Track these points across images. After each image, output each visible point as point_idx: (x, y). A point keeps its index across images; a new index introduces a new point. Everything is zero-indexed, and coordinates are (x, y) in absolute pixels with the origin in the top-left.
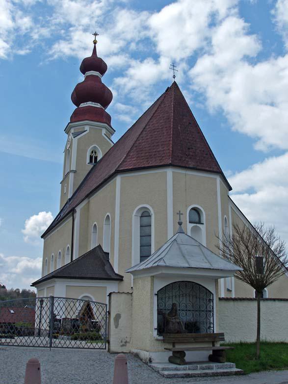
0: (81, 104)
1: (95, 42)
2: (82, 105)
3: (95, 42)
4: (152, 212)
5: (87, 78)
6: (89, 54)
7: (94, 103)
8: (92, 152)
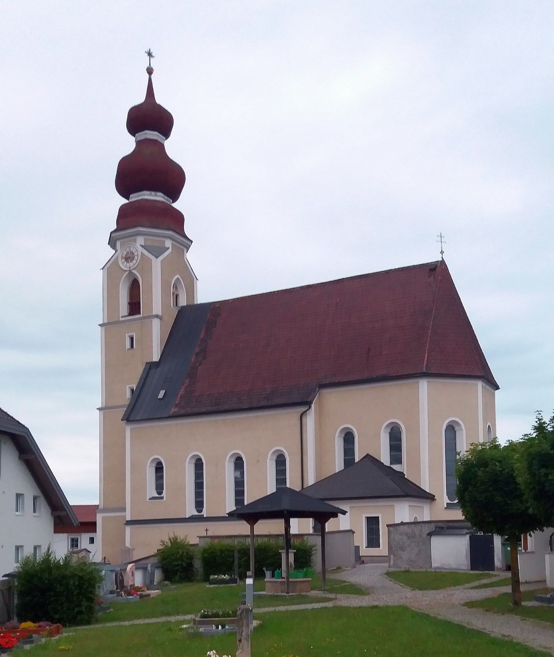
1: (150, 71)
2: (135, 197)
3: (150, 71)
5: (138, 143)
6: (140, 98)
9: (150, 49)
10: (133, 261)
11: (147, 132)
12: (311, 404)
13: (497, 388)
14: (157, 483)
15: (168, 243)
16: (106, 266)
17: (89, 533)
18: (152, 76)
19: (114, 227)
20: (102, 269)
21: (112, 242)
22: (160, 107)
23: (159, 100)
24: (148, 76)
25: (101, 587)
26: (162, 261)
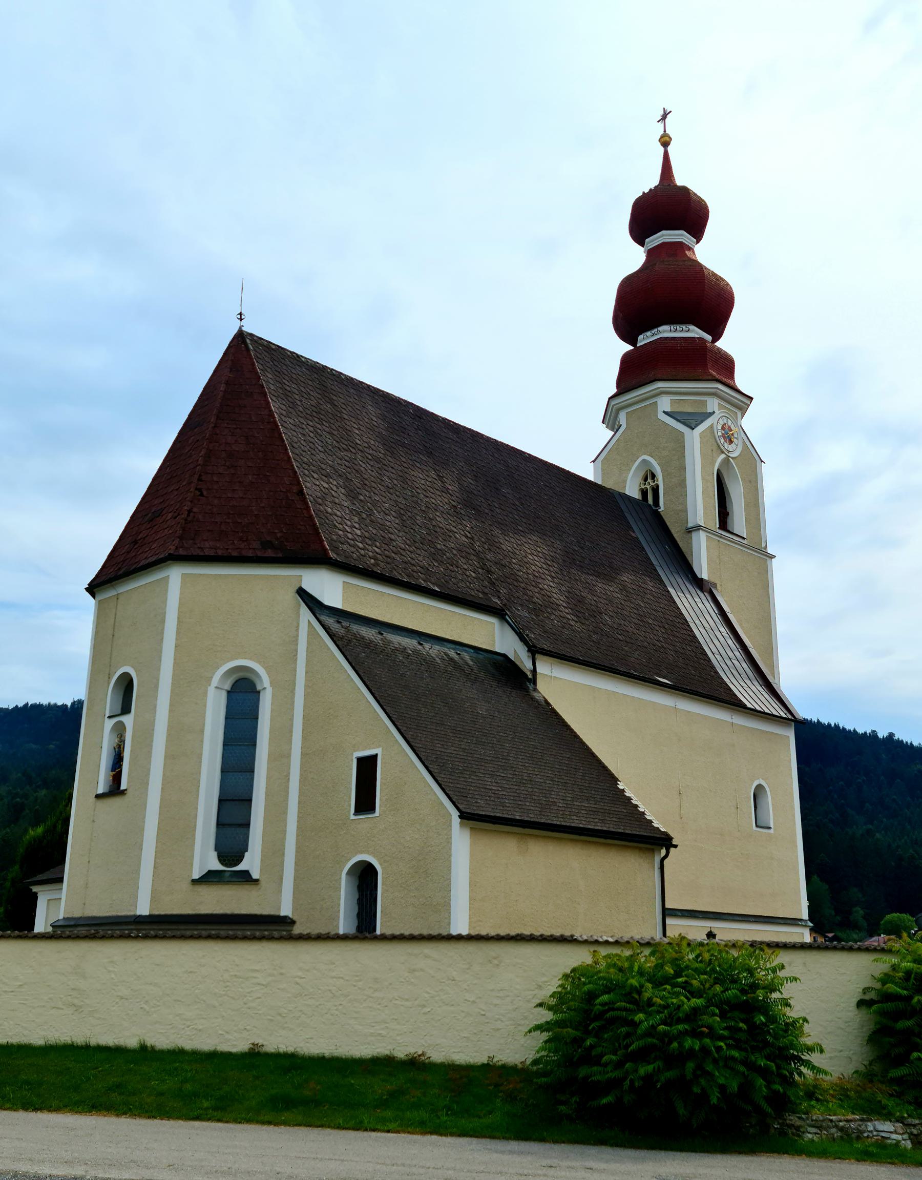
0: (640, 337)
1: (665, 142)
2: (644, 339)
3: (665, 142)
4: (265, 682)
5: (650, 253)
6: (651, 180)
7: (649, 334)
8: (646, 479)
9: (658, 122)
10: (286, 917)
11: (664, 232)
12: (631, 803)
13: (665, 842)
14: (381, 808)
15: (713, 404)
16: (605, 449)
17: (20, 705)
18: (669, 149)
19: (614, 390)
20: (594, 461)
21: (610, 419)
22: (685, 191)
23: (680, 180)
24: (662, 149)
25: (831, 1140)
26: (702, 435)
